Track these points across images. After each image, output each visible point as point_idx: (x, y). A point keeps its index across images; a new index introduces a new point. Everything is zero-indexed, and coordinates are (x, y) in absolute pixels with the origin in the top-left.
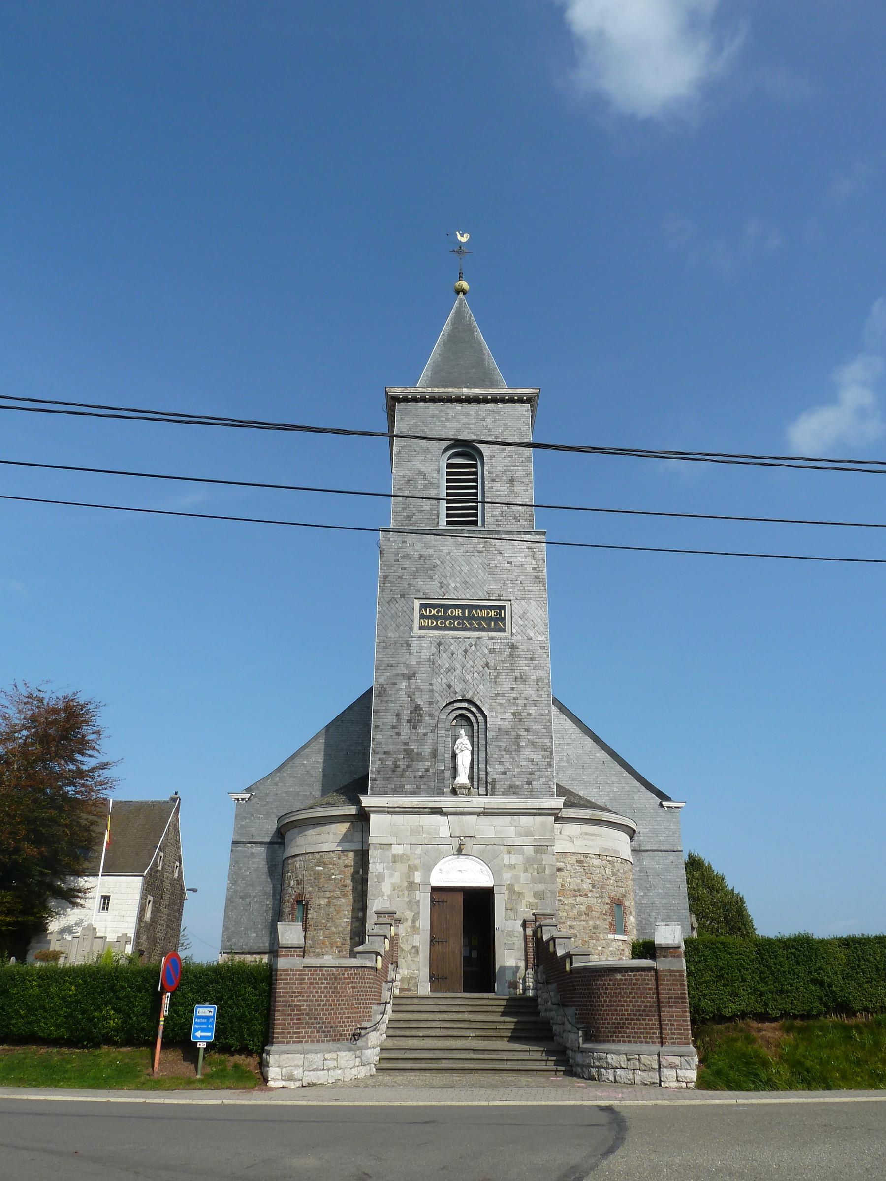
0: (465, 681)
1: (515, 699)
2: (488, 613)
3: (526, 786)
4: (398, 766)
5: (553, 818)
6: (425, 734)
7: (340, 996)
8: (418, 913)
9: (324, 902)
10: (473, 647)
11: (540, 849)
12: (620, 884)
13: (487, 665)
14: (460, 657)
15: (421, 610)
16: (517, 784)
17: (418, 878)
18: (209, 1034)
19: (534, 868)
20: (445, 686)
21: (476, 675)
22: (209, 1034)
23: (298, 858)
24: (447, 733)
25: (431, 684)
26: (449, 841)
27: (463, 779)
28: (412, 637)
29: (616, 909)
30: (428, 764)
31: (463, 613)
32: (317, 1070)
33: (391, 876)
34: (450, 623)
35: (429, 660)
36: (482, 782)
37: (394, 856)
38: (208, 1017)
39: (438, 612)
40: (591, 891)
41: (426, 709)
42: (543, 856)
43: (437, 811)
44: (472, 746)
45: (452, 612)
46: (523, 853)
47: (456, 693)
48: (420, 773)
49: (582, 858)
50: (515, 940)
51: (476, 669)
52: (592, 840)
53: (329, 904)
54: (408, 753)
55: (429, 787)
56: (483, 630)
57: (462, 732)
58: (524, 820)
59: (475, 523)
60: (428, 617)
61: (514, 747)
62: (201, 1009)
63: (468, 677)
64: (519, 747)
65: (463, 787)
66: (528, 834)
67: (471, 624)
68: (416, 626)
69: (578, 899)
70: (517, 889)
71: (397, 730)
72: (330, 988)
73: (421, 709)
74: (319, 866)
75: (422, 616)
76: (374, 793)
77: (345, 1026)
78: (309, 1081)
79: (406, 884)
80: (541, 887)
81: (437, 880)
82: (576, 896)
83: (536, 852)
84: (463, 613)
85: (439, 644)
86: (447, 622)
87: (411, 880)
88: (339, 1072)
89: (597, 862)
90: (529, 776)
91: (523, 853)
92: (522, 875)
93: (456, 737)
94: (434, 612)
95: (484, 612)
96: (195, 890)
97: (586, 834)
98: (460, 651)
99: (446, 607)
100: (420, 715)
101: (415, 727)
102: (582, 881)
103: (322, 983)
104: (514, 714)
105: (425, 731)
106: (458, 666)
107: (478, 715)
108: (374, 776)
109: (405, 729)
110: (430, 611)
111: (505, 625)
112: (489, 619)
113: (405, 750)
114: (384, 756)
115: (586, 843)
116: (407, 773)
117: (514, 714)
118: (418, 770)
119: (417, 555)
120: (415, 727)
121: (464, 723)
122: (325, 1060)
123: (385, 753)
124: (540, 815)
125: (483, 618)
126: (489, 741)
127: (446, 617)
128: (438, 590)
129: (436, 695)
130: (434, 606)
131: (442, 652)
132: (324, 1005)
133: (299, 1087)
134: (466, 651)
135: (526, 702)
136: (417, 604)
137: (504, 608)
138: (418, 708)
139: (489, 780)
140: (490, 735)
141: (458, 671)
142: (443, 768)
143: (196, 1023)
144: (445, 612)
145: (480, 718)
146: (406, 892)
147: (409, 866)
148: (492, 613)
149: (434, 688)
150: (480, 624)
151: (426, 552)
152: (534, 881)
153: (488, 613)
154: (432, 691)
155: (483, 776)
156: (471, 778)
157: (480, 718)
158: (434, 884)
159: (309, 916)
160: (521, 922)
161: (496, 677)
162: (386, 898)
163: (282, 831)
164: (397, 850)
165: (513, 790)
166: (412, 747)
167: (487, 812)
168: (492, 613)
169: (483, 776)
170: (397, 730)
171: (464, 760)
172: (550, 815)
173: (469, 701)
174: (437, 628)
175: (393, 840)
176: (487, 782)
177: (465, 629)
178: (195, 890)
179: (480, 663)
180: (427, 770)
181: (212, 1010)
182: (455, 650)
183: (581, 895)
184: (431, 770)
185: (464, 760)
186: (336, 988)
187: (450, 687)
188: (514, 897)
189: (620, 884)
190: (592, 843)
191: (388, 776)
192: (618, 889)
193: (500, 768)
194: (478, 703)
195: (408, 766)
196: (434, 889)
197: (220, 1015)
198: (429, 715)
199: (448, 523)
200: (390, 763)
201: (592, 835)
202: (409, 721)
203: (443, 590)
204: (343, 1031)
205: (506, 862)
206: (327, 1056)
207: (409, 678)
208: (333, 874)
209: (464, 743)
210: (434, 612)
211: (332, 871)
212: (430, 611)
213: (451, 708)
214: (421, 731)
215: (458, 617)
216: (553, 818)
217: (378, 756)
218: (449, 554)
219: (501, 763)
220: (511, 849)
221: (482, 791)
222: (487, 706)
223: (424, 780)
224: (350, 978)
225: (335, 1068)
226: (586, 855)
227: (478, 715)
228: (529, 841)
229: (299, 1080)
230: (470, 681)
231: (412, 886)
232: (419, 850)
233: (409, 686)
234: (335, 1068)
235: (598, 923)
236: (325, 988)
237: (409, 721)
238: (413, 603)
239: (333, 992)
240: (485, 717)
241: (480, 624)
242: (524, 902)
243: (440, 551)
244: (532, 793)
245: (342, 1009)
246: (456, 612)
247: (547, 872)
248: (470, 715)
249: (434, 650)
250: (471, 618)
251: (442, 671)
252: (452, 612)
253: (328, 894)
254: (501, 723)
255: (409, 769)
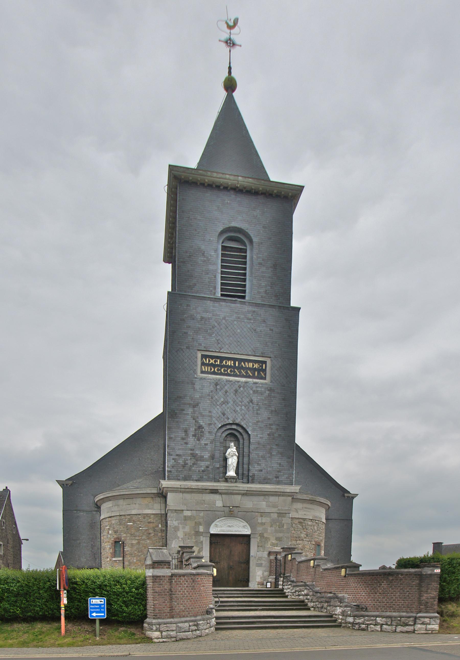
0: (235, 411)
1: (270, 425)
2: (253, 366)
3: (275, 479)
4: (187, 464)
5: (290, 498)
6: (206, 444)
7: (197, 591)
8: (202, 548)
9: (134, 542)
10: (242, 389)
11: (281, 514)
12: (320, 535)
13: (251, 401)
14: (232, 394)
15: (202, 359)
16: (269, 477)
17: (201, 529)
18: (103, 614)
19: (277, 525)
20: (220, 414)
21: (243, 407)
22: (103, 614)
23: (113, 518)
24: (221, 444)
25: (210, 412)
26: (222, 509)
27: (231, 473)
28: (196, 378)
29: (317, 547)
30: (208, 463)
31: (235, 364)
32: (185, 632)
33: (184, 528)
34: (224, 371)
35: (209, 395)
36: (243, 474)
37: (185, 517)
38: (100, 605)
39: (215, 361)
40: (305, 538)
41: (206, 429)
42: (283, 518)
43: (214, 491)
44: (239, 453)
45: (226, 363)
46: (270, 517)
47: (228, 419)
48: (203, 469)
49: (302, 521)
50: (263, 562)
51: (243, 403)
52: (309, 512)
53: (139, 543)
54: (194, 456)
55: (209, 477)
56: (249, 377)
57: (232, 444)
58: (272, 499)
59: (244, 297)
60: (208, 365)
61: (268, 455)
62: (94, 600)
63: (238, 409)
64: (272, 455)
65: (232, 478)
66: (275, 506)
67: (239, 372)
68: (199, 371)
69: (298, 542)
70: (265, 535)
71: (185, 441)
72: (190, 586)
73: (203, 428)
74: (130, 522)
75: (203, 364)
76: (169, 479)
77: (200, 608)
78: (181, 637)
79: (193, 532)
80: (280, 535)
81: (213, 530)
82: (297, 540)
83: (278, 517)
84: (235, 364)
85: (216, 384)
86: (222, 370)
87: (197, 530)
88: (198, 632)
89: (310, 523)
90: (277, 473)
91: (270, 517)
92: (269, 528)
93: (228, 448)
94: (212, 361)
95: (251, 365)
96: (27, 540)
97: (306, 508)
98: (232, 390)
99: (222, 359)
100: (202, 432)
101: (199, 440)
102: (301, 533)
103: (185, 584)
104: (269, 435)
105: (206, 442)
106: (230, 400)
107: (244, 434)
108: (169, 469)
109: (191, 440)
110: (209, 361)
111: (265, 375)
112: (253, 370)
113: (191, 454)
114: (177, 457)
115: (305, 513)
116: (193, 468)
117: (269, 435)
118: (201, 466)
119: (199, 317)
120: (199, 440)
121: (232, 439)
122: (190, 626)
123: (177, 455)
124: (283, 496)
125: (249, 369)
126: (251, 450)
127: (222, 366)
128: (216, 345)
129: (214, 419)
130: (212, 357)
131: (218, 390)
132: (187, 596)
133: (174, 641)
134: (236, 391)
135: (278, 427)
136: (199, 355)
137: (265, 362)
138: (200, 427)
139: (250, 474)
140: (252, 447)
141: (230, 404)
142: (218, 466)
143: (91, 608)
144: (221, 362)
145: (245, 436)
146: (194, 537)
147: (196, 522)
148: (256, 366)
149: (213, 414)
150: (247, 373)
151: (205, 315)
152: (276, 531)
153: (253, 366)
154: (211, 416)
155: (245, 472)
156: (237, 473)
157: (245, 436)
158: (212, 532)
159: (125, 549)
160: (267, 553)
161: (257, 410)
162: (180, 539)
163: (98, 504)
164: (188, 513)
165: (266, 481)
166: (197, 452)
167: (247, 494)
168: (256, 366)
169: (245, 472)
170: (185, 441)
171: (232, 461)
172: (289, 496)
173: (238, 425)
174: (214, 373)
175: (184, 508)
176: (248, 476)
177: (236, 376)
178: (27, 540)
179: (246, 400)
180: (207, 467)
181: (103, 600)
182: (228, 390)
183: (300, 540)
184: (210, 467)
185: (232, 461)
186: (194, 586)
187: (224, 414)
188: (263, 540)
189: (320, 535)
190: (308, 513)
191: (179, 470)
192: (319, 537)
193: (259, 468)
194: (245, 426)
195: (194, 464)
196: (212, 535)
197: (109, 603)
198: (209, 432)
199: (222, 295)
200: (181, 462)
201: (309, 509)
202: (194, 436)
203: (219, 345)
204: (199, 610)
205: (260, 521)
206: (191, 624)
207: (194, 407)
208: (140, 527)
209: (232, 450)
210: (212, 361)
211: (140, 525)
212: (209, 361)
213: (224, 429)
214: (203, 442)
215: (230, 367)
216: (290, 498)
217: (172, 457)
218: (224, 318)
219: (259, 464)
220: (263, 514)
221: (245, 480)
222: (250, 428)
223: (205, 473)
224: (201, 581)
225: (196, 630)
226: (304, 519)
227: (244, 434)
228: (275, 510)
229: (174, 637)
230: (239, 411)
231: (197, 533)
232: (202, 514)
233: (194, 412)
234: (196, 630)
235: (308, 553)
236: (187, 587)
237: (194, 436)
238: (196, 353)
239: (192, 589)
240: (249, 435)
241: (247, 373)
242: (269, 543)
243: (219, 315)
244: (278, 483)
245: (198, 598)
246: (229, 363)
247: (285, 527)
248: (237, 434)
249: (212, 388)
250: (240, 368)
251: (218, 403)
252: (226, 363)
253: (137, 538)
254: (260, 440)
255: (195, 466)
